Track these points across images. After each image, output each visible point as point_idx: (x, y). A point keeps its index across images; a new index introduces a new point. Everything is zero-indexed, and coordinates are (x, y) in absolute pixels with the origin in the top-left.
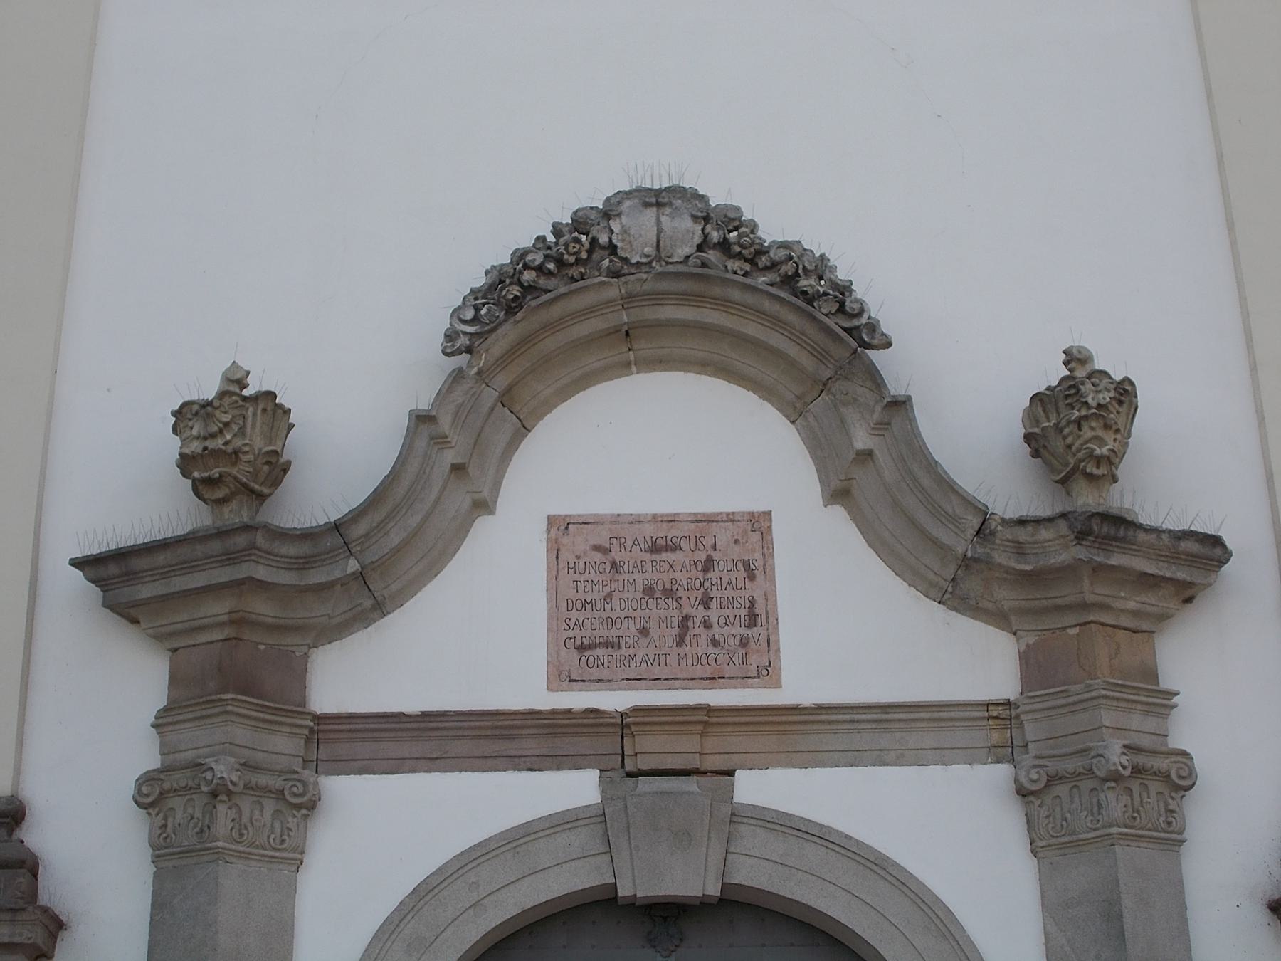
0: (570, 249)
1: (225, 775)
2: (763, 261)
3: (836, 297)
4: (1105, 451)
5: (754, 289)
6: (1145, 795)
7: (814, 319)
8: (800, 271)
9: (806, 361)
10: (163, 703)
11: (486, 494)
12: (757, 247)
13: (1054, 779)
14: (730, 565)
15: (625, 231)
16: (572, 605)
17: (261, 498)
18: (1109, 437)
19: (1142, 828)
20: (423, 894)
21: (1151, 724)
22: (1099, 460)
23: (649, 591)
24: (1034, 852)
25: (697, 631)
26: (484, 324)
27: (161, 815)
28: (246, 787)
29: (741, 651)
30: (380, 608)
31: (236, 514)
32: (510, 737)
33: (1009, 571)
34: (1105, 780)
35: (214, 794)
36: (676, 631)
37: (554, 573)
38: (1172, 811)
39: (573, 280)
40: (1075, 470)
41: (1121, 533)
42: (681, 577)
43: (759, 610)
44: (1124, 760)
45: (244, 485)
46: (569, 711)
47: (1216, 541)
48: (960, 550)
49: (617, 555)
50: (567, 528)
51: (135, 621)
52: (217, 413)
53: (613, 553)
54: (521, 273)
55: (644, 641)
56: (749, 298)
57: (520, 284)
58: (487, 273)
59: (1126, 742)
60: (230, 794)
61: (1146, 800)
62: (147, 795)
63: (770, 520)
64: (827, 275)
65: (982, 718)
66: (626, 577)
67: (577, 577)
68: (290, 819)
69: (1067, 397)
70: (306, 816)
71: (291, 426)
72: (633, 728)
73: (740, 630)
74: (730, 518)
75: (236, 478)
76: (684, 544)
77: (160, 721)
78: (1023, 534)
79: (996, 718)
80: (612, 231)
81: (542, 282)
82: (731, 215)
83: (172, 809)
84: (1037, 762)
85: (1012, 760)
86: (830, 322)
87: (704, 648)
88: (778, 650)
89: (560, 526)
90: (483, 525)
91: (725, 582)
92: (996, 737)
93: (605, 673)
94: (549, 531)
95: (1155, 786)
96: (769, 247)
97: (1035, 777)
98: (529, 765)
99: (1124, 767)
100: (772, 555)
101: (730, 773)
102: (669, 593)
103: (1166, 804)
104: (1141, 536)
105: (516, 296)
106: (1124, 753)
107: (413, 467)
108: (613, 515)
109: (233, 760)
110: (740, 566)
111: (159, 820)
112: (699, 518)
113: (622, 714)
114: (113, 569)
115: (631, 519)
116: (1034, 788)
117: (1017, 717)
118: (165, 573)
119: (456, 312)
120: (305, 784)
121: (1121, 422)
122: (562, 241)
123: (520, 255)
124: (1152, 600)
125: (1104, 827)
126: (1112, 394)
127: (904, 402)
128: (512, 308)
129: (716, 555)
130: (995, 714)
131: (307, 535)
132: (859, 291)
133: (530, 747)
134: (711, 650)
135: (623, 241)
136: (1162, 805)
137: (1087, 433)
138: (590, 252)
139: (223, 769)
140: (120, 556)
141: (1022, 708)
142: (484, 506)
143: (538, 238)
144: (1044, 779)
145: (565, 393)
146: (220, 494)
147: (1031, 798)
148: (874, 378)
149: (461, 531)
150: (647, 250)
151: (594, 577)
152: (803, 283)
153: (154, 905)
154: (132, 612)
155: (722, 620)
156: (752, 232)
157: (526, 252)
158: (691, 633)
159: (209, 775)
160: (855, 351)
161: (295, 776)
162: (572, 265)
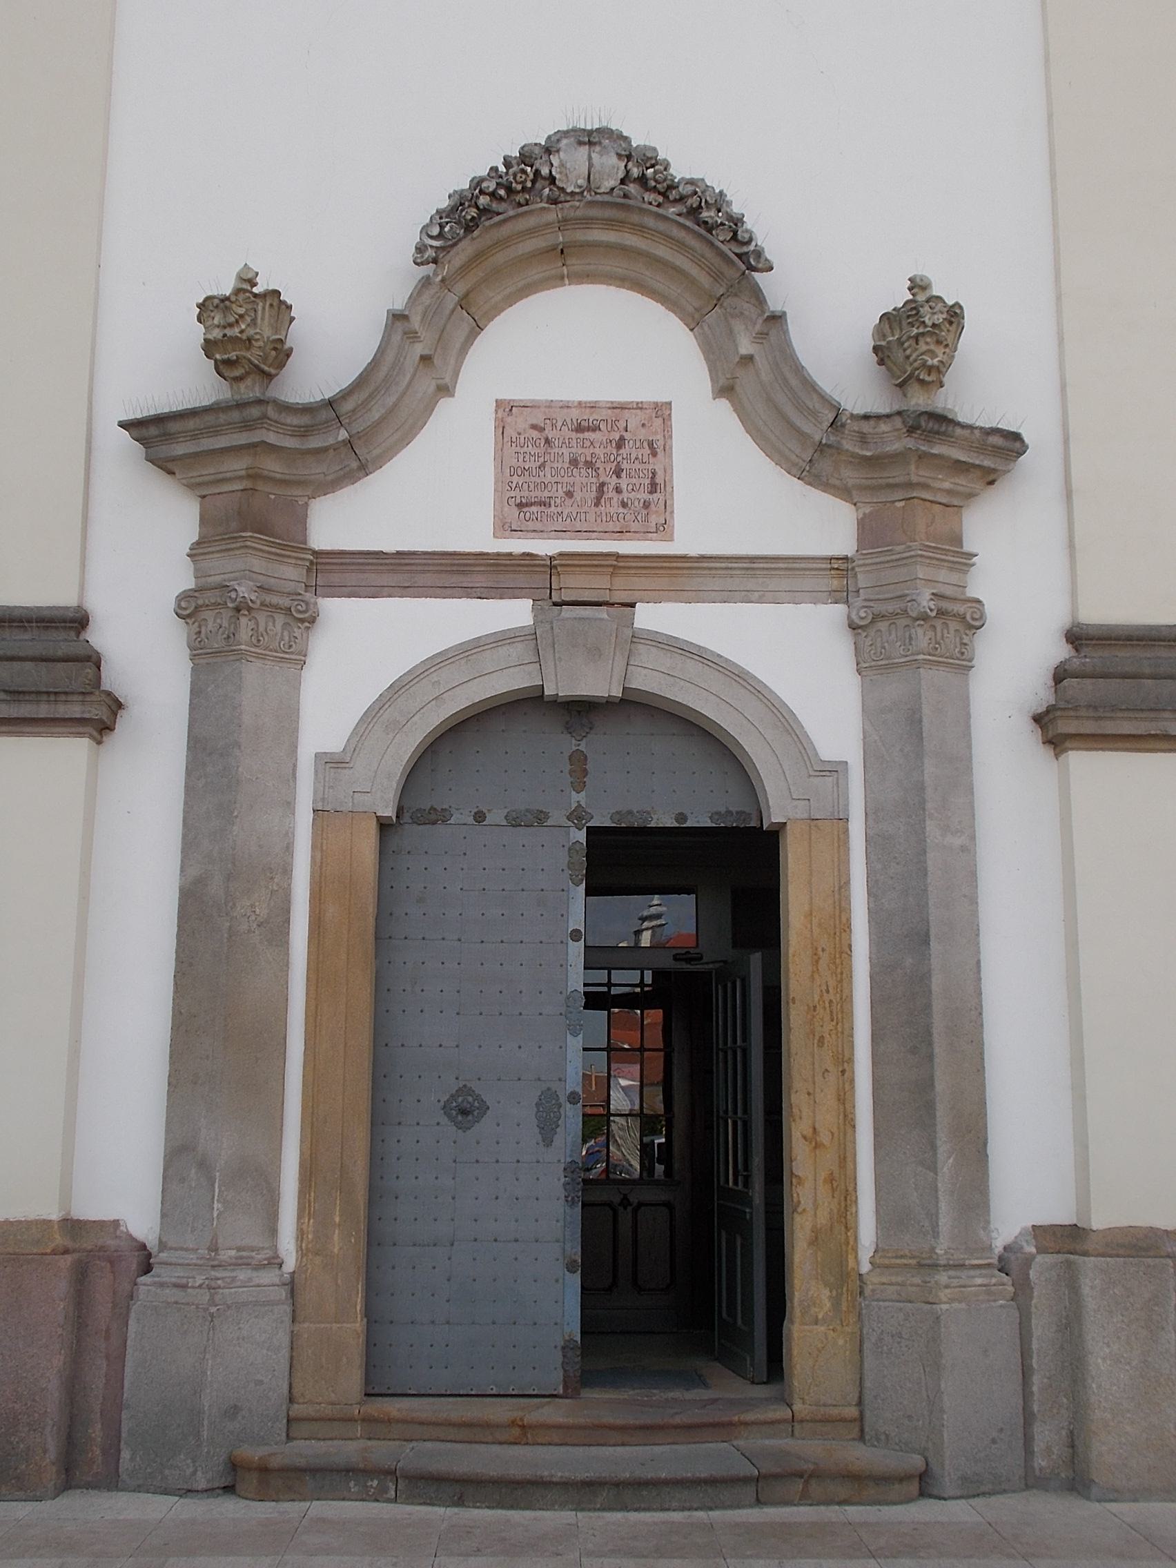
0: (518, 178)
2: (673, 195)
3: (730, 227)
4: (935, 361)
5: (665, 218)
6: (945, 631)
7: (712, 244)
8: (703, 204)
9: (704, 280)
10: (196, 538)
12: (669, 182)
13: (877, 618)
14: (638, 444)
15: (562, 165)
16: (514, 471)
17: (270, 377)
18: (940, 351)
19: (941, 656)
20: (398, 689)
21: (954, 578)
22: (930, 369)
23: (574, 462)
24: (859, 672)
26: (446, 239)
28: (262, 604)
30: (364, 469)
31: (250, 390)
33: (854, 455)
35: (238, 610)
36: (594, 494)
38: (965, 644)
39: (520, 205)
41: (943, 429)
42: (599, 452)
43: (659, 480)
44: (932, 604)
46: (510, 554)
47: (1016, 437)
48: (817, 438)
49: (550, 433)
50: (511, 410)
52: (234, 306)
53: (546, 431)
54: (477, 197)
55: (569, 502)
56: (662, 226)
58: (450, 196)
59: (934, 591)
60: (249, 609)
61: (946, 635)
62: (185, 609)
64: (724, 208)
66: (556, 450)
67: (518, 449)
68: (296, 630)
69: (909, 317)
71: (292, 319)
72: (559, 569)
74: (639, 406)
75: (249, 361)
77: (194, 552)
78: (866, 427)
80: (552, 165)
81: (495, 206)
85: (847, 602)
86: (724, 248)
87: (615, 508)
89: (506, 408)
90: (444, 405)
91: (633, 457)
92: (835, 583)
93: (538, 526)
94: (496, 412)
96: (679, 183)
97: (863, 615)
98: (479, 595)
99: (931, 610)
101: (633, 605)
102: (589, 465)
103: (961, 639)
104: (958, 431)
106: (932, 599)
107: (390, 357)
108: (547, 401)
110: (645, 444)
111: (195, 628)
112: (615, 405)
114: (153, 431)
118: (195, 436)
120: (307, 604)
122: (511, 171)
123: (477, 183)
126: (945, 316)
127: (780, 317)
128: (470, 227)
129: (627, 436)
130: (836, 566)
131: (307, 409)
132: (749, 223)
133: (480, 580)
134: (621, 510)
135: (561, 173)
136: (958, 639)
137: (923, 347)
138: (534, 182)
139: (244, 591)
140: (159, 420)
142: (445, 390)
143: (491, 169)
144: (870, 617)
145: (511, 300)
146: (238, 372)
148: (757, 296)
149: (429, 409)
150: (580, 182)
152: (705, 214)
155: (630, 487)
156: (665, 169)
157: (482, 180)
159: (233, 595)
160: (744, 273)
161: (299, 597)
162: (519, 192)
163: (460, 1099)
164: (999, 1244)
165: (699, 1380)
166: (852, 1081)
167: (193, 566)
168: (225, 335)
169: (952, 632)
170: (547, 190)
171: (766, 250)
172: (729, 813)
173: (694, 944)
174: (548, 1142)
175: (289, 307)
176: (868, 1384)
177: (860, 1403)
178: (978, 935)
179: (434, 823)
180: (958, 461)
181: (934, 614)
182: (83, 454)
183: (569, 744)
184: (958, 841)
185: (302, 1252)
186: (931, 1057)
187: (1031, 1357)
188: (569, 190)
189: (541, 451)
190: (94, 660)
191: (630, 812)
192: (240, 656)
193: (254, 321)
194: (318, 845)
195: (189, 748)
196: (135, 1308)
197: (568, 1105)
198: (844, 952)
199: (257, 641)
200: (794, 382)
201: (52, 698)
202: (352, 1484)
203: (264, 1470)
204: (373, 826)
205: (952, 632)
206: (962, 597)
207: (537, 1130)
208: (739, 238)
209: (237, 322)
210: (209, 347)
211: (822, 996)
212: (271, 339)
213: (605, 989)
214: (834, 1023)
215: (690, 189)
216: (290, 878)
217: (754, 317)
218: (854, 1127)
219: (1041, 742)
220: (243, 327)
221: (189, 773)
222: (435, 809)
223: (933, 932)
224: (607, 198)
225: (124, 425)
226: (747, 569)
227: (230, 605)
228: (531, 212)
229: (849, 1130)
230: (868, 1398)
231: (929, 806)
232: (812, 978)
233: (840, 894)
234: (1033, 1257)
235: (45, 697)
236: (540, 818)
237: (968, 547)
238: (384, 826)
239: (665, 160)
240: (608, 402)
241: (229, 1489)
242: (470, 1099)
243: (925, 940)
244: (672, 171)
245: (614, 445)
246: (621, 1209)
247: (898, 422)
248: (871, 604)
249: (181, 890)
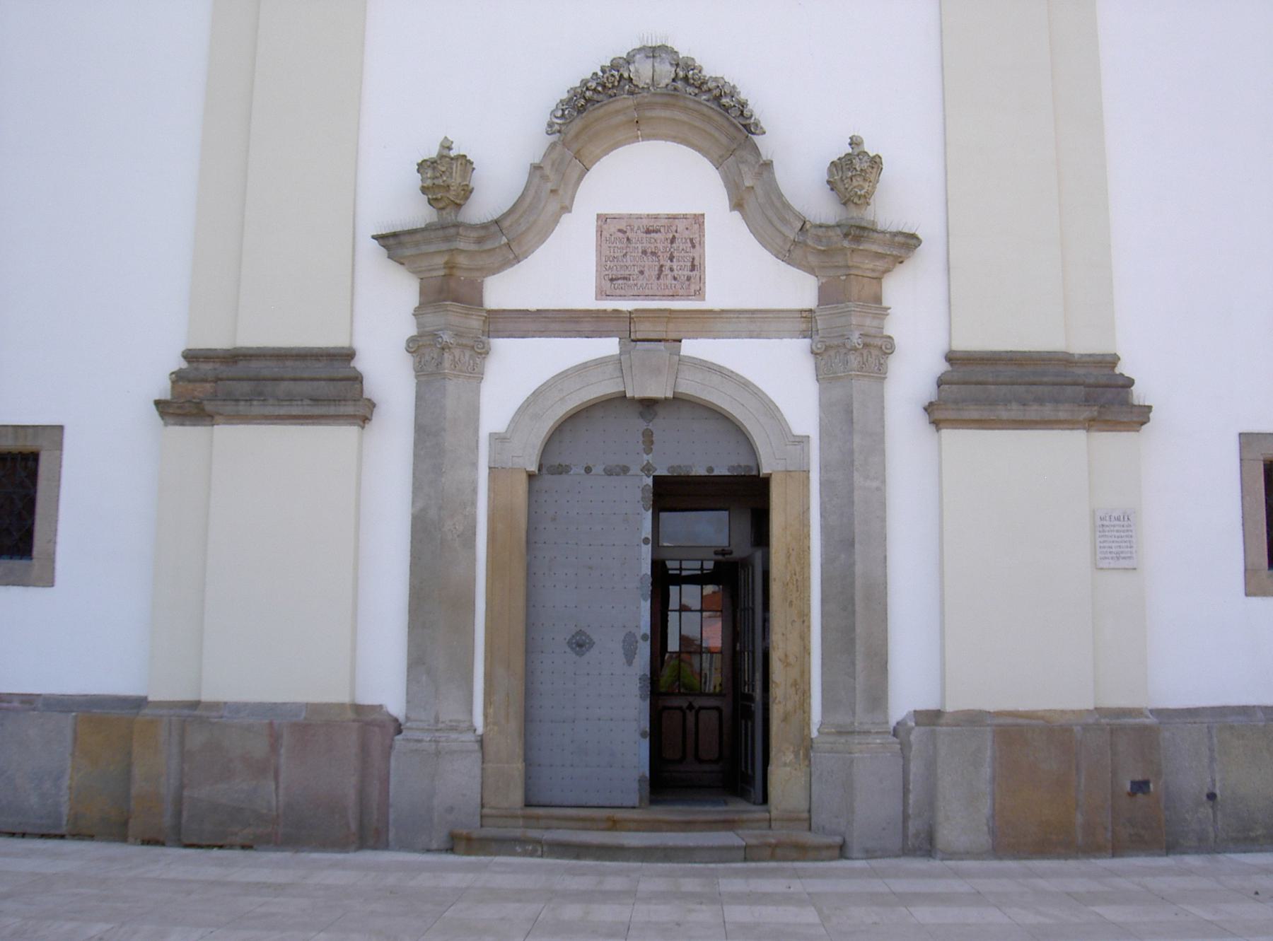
0: (610, 81)
1: (448, 341)
2: (705, 88)
3: (739, 108)
4: (863, 192)
5: (700, 103)
6: (869, 356)
7: (728, 119)
8: (723, 93)
9: (724, 140)
10: (417, 304)
11: (567, 203)
12: (702, 81)
13: (827, 348)
14: (684, 240)
15: (637, 71)
16: (608, 258)
17: (459, 206)
18: (866, 185)
19: (866, 372)
20: (537, 394)
21: (875, 323)
22: (860, 197)
23: (644, 252)
24: (818, 380)
25: (666, 273)
26: (566, 119)
27: (419, 356)
28: (458, 344)
29: (687, 283)
30: (517, 259)
31: (449, 216)
32: (577, 322)
33: (814, 248)
34: (851, 350)
35: (443, 349)
36: (657, 272)
37: (599, 243)
38: (882, 364)
39: (611, 96)
40: (849, 200)
41: (866, 234)
42: (660, 246)
43: (696, 263)
44: (860, 341)
45: (452, 201)
46: (605, 311)
47: (913, 236)
48: (792, 238)
49: (629, 234)
50: (606, 221)
51: (402, 264)
52: (439, 167)
53: (628, 234)
54: (585, 92)
55: (641, 277)
56: (697, 107)
57: (584, 98)
58: (568, 92)
59: (862, 332)
60: (449, 348)
61: (869, 359)
62: (412, 348)
63: (704, 218)
64: (736, 96)
65: (798, 318)
66: (634, 245)
67: (610, 245)
68: (477, 359)
69: (847, 164)
70: (484, 358)
71: (474, 169)
72: (635, 319)
73: (687, 273)
74: (685, 217)
75: (448, 198)
76: (662, 230)
77: (417, 313)
78: (820, 232)
79: (805, 317)
80: (630, 71)
81: (595, 97)
82: (690, 63)
83: (424, 354)
84: (822, 339)
85: (811, 337)
86: (736, 121)
87: (669, 281)
88: (704, 283)
89: (603, 219)
90: (565, 218)
91: (681, 248)
92: (804, 326)
93: (623, 292)
94: (597, 221)
95: (875, 352)
96: (708, 80)
97: (819, 346)
98: (587, 335)
99: (859, 344)
100: (704, 236)
101: (680, 341)
102: (653, 254)
103: (879, 361)
104: (876, 235)
105: (582, 105)
106: (860, 338)
107: (532, 192)
108: (628, 214)
109: (451, 333)
110: (688, 241)
111: (418, 359)
112: (670, 216)
113: (630, 312)
114: (391, 241)
115: (637, 216)
116: (819, 351)
117: (815, 317)
118: (417, 244)
119: (553, 113)
120: (483, 343)
121: (872, 177)
122: (605, 76)
123: (584, 83)
124: (880, 264)
125: (848, 371)
126: (868, 164)
127: (769, 164)
128: (581, 109)
129: (677, 235)
130: (804, 315)
131: (484, 226)
132: (751, 105)
133: (587, 327)
134: (673, 282)
135: (636, 76)
136: (877, 361)
137: (854, 183)
138: (619, 82)
139: (447, 337)
140: (395, 235)
141: (817, 314)
142: (567, 209)
143: (594, 74)
144: (824, 347)
145: (606, 152)
146: (441, 205)
147: (818, 356)
148: (755, 149)
149: (556, 221)
150: (648, 81)
151: (619, 245)
152: (724, 101)
153: (417, 397)
154: (402, 261)
155: (679, 267)
156: (700, 72)
157: (587, 81)
158: (664, 273)
159: (440, 340)
160: (747, 137)
161: (479, 340)
162: (610, 89)
163: (578, 638)
164: (893, 722)
165: (726, 803)
166: (809, 627)
167: (415, 321)
168: (434, 184)
169: (874, 357)
170: (627, 87)
171: (761, 122)
172: (739, 466)
173: (727, 545)
174: (630, 662)
175: (472, 163)
176: (814, 799)
177: (809, 811)
178: (885, 540)
179: (561, 473)
180: (876, 253)
181: (861, 347)
183: (641, 425)
184: (875, 484)
185: (486, 724)
186: (853, 613)
187: (909, 784)
188: (641, 87)
189: (624, 246)
190: (357, 379)
191: (680, 467)
192: (444, 377)
193: (451, 173)
194: (492, 490)
195: (415, 432)
196: (394, 753)
197: (641, 641)
198: (806, 550)
199: (455, 363)
200: (779, 205)
201: (337, 403)
202: (517, 848)
203: (469, 839)
204: (524, 477)
205: (874, 357)
206: (880, 335)
207: (623, 656)
208: (745, 115)
209: (441, 175)
210: (424, 190)
211: (791, 577)
212: (462, 184)
213: (678, 572)
214: (799, 593)
215: (714, 84)
216: (476, 508)
217: (753, 163)
218: (809, 654)
219: (928, 421)
220: (445, 178)
221: (416, 445)
222: (562, 466)
223: (856, 540)
224: (664, 91)
225: (374, 237)
226: (750, 318)
227: (439, 346)
228: (618, 100)
229: (807, 656)
230: (813, 809)
231: (856, 463)
232: (786, 567)
233: (803, 516)
234: (913, 728)
235: (333, 403)
236: (625, 470)
237: (885, 304)
238: (531, 476)
239: (700, 66)
240: (665, 214)
241: (451, 850)
242: (584, 638)
243: (852, 544)
244: (704, 73)
245: (669, 241)
246: (688, 711)
247: (838, 231)
248: (825, 340)
249: (412, 515)
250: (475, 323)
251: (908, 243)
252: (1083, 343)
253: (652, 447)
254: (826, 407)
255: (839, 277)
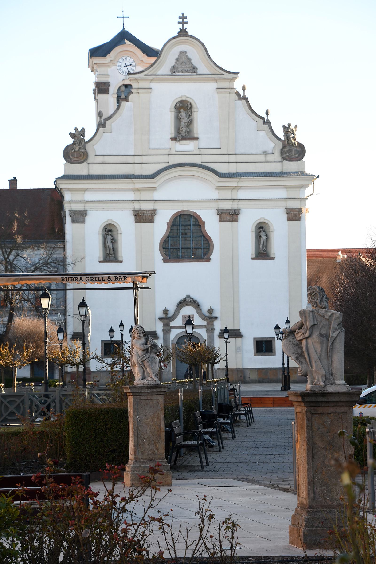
182: (225, 348)
250: (169, 328)
251: (216, 318)
252: (236, 328)
253: (187, 54)
254: (207, 336)
255: (22, 425)
